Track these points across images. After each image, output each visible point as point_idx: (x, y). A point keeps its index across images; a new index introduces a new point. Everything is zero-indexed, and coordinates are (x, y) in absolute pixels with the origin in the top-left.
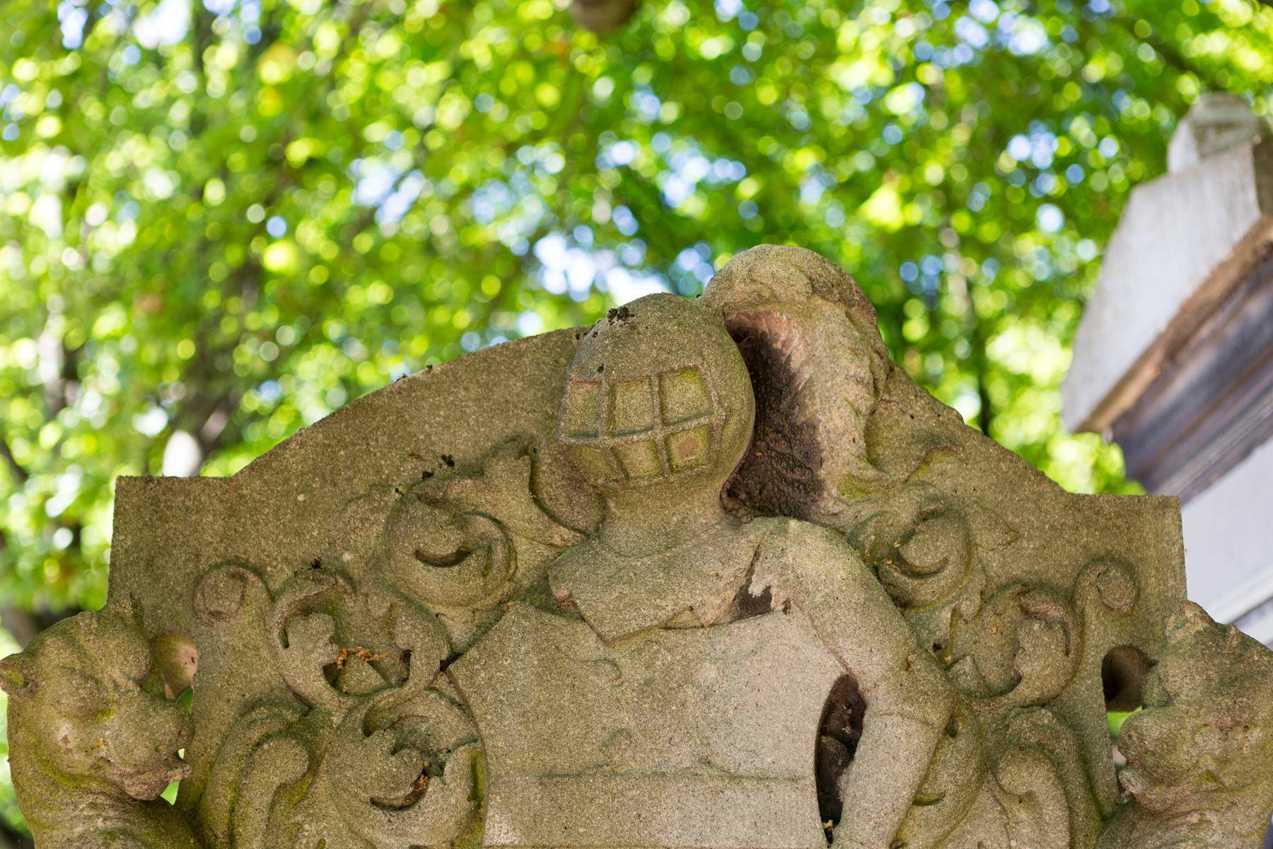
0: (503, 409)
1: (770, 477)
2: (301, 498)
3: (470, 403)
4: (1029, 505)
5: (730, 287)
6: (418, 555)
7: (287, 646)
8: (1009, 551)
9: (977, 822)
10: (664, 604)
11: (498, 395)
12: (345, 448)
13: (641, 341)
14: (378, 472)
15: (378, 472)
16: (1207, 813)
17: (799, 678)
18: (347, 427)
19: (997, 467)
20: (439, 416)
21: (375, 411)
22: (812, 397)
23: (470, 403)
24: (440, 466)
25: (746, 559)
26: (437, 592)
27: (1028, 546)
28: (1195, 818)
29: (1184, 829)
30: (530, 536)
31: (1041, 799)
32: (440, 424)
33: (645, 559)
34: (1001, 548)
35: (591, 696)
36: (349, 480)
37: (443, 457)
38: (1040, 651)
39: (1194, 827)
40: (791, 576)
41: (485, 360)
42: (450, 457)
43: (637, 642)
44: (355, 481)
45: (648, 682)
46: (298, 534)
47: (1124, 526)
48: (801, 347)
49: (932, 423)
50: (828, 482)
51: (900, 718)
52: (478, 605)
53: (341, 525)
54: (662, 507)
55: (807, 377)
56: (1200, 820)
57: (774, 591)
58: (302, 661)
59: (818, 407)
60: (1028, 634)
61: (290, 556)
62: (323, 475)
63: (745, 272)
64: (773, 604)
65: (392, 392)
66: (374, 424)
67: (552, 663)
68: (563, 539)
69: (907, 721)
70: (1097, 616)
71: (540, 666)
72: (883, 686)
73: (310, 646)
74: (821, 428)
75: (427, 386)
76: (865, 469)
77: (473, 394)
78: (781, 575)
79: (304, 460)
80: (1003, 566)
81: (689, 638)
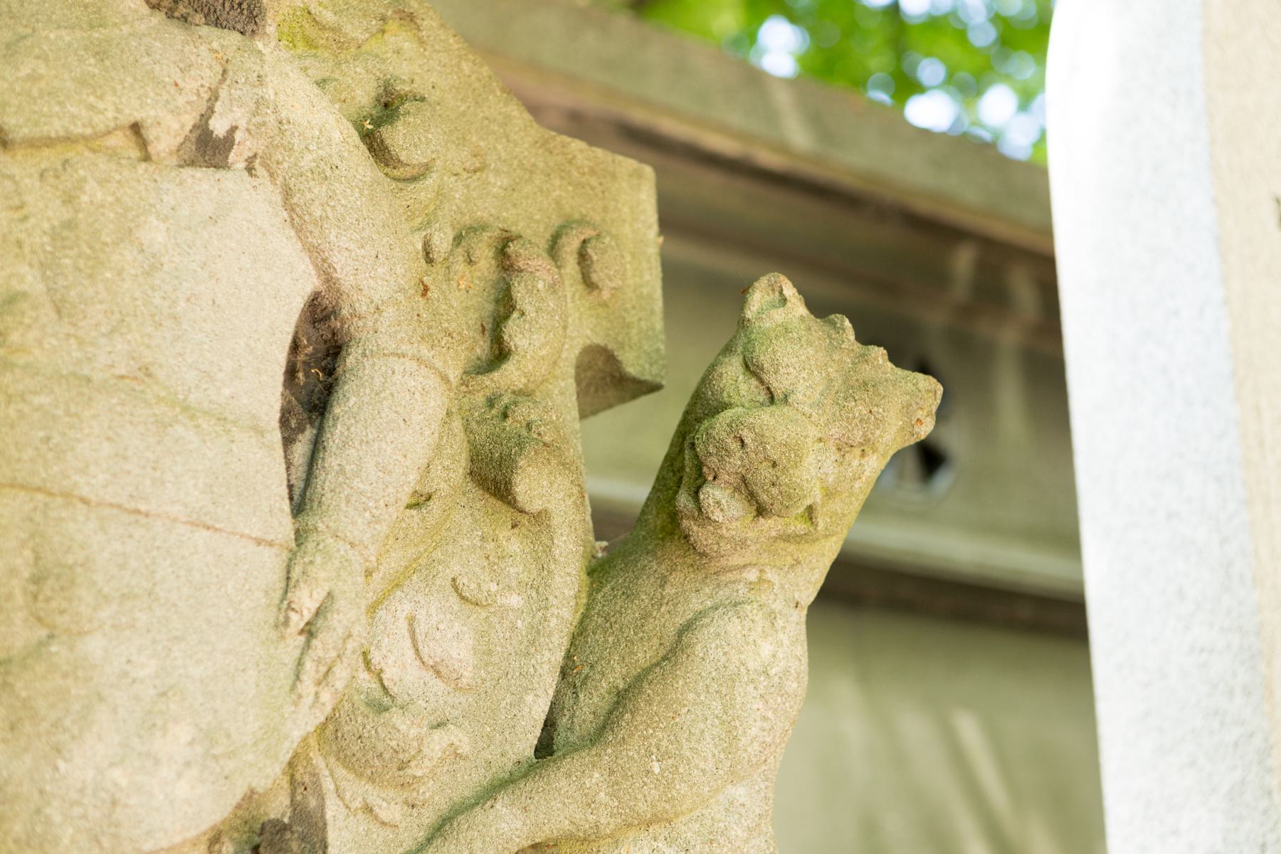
9: (450, 548)
10: (101, 105)
16: (767, 569)
19: (458, 66)
25: (210, 76)
27: (497, 183)
28: (752, 575)
29: (742, 590)
31: (556, 521)
33: (63, 32)
34: (465, 175)
39: (751, 586)
40: (271, 119)
43: (49, 158)
45: (69, 225)
47: (599, 189)
50: (270, 14)
51: (415, 364)
56: (760, 578)
57: (238, 136)
60: (530, 292)
64: (232, 156)
69: (424, 371)
72: (390, 312)
76: (326, 8)
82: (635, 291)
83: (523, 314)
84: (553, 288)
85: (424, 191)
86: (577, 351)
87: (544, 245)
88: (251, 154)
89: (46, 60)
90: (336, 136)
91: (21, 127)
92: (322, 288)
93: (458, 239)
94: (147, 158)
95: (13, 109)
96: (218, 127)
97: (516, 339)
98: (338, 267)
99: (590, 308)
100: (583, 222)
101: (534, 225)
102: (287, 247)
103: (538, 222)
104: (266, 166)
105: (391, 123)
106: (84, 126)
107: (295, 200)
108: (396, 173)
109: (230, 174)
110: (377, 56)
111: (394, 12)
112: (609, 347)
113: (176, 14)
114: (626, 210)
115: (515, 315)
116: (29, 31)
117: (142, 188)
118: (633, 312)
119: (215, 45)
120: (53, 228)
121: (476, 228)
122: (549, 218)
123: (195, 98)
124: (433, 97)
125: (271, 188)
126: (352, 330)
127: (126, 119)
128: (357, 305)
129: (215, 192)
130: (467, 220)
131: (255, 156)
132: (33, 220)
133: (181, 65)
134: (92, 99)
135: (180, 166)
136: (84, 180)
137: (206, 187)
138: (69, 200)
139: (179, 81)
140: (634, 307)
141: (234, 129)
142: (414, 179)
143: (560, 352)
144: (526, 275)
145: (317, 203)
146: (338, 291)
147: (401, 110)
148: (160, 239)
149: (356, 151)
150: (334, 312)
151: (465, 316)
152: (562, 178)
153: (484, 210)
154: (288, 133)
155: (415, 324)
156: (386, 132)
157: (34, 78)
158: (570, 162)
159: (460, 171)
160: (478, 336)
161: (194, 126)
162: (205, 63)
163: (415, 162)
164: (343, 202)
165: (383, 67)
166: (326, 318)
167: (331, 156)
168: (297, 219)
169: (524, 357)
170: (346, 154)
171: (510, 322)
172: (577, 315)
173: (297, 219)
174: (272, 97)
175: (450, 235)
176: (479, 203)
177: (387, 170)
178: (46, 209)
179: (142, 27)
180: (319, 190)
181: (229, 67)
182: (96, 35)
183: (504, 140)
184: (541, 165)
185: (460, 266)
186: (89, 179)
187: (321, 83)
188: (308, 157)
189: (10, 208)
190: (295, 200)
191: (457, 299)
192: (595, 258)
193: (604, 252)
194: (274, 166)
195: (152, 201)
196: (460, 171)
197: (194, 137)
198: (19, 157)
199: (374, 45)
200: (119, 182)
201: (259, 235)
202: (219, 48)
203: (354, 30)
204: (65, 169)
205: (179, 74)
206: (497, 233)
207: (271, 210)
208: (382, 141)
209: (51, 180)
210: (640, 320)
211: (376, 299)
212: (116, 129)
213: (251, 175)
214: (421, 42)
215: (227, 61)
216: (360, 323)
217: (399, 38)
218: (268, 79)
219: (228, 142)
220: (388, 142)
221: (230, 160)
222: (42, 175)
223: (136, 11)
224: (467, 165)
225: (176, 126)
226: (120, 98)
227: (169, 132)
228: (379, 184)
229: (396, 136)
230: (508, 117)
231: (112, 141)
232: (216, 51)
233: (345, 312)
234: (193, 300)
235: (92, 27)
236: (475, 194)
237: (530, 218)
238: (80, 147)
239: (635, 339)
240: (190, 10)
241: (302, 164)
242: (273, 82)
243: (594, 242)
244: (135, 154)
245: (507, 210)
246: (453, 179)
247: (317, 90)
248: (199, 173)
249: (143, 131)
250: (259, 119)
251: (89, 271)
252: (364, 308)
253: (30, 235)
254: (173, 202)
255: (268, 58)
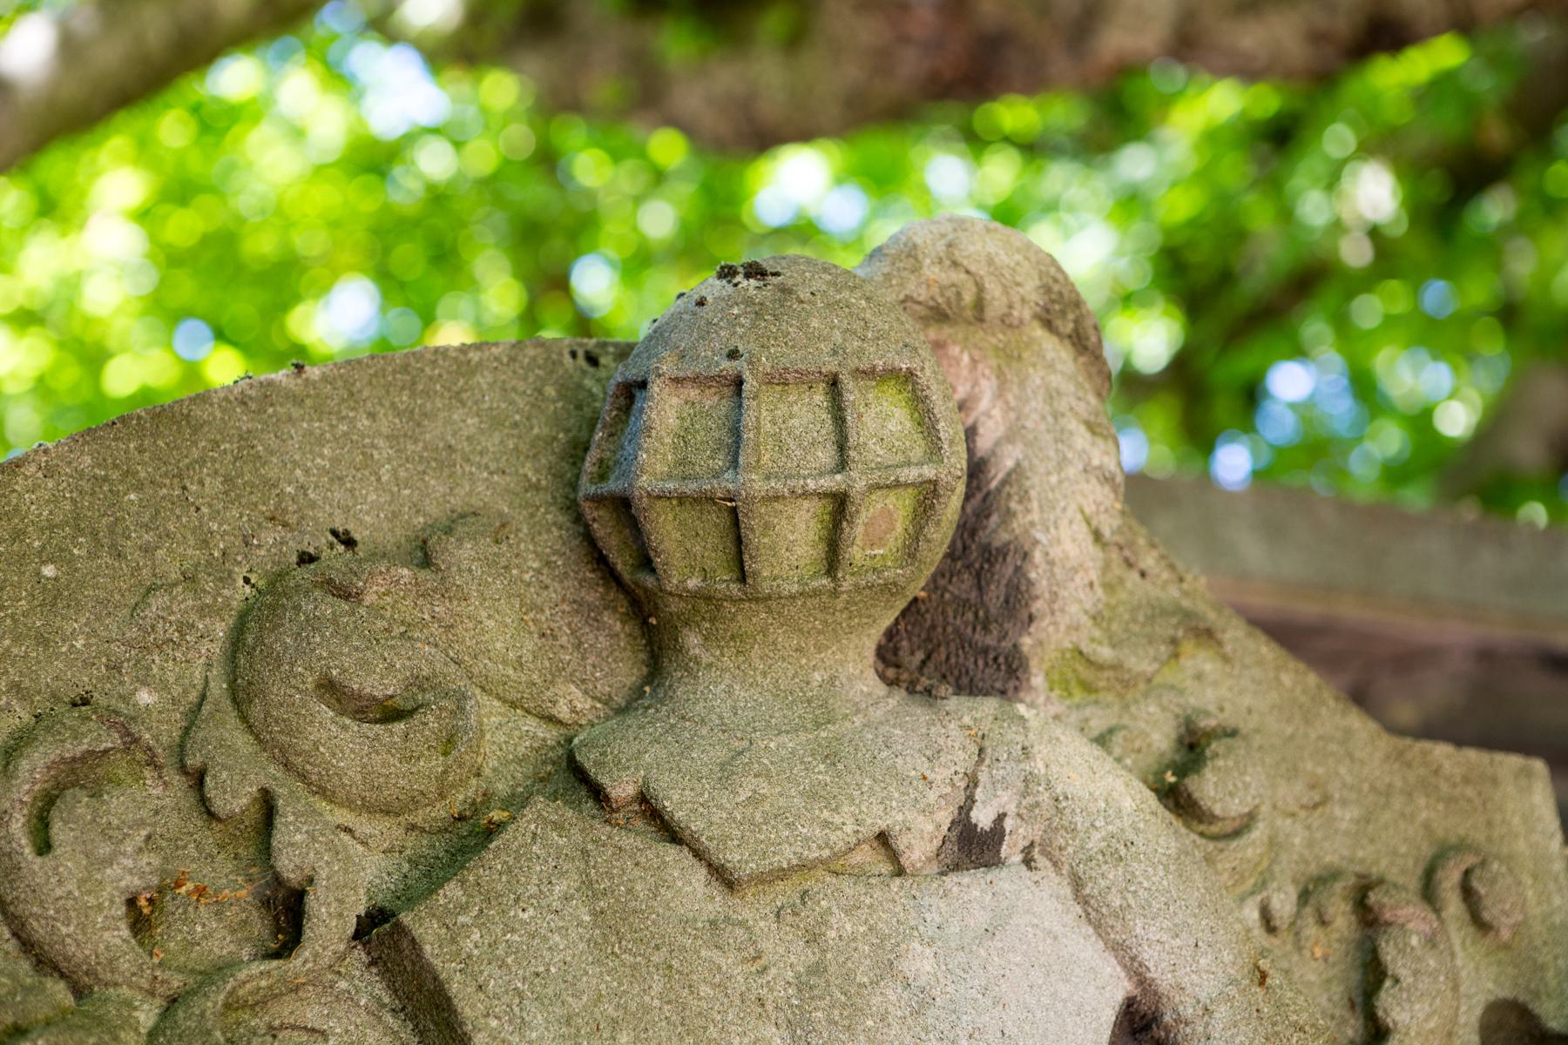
0: (444, 459)
1: (576, 779)
2: (49, 571)
3: (381, 442)
4: (1333, 747)
5: (915, 270)
6: (330, 689)
7: (44, 846)
8: (1316, 819)
10: (837, 820)
11: (433, 432)
12: (139, 487)
13: (809, 314)
14: (205, 543)
15: (205, 543)
17: (1064, 990)
18: (141, 451)
19: (1277, 678)
20: (322, 456)
21: (196, 430)
22: (1024, 498)
23: (381, 442)
24: (332, 547)
25: (962, 759)
26: (354, 775)
27: (1346, 816)
30: (514, 695)
32: (323, 471)
33: (784, 738)
34: (1303, 814)
35: (705, 990)
36: (147, 550)
37: (334, 533)
38: (1424, 984)
40: (1045, 798)
41: (405, 368)
42: (347, 532)
43: (785, 893)
44: (160, 553)
45: (817, 969)
46: (43, 641)
47: (1477, 801)
48: (996, 413)
49: (1174, 591)
50: (1034, 664)
52: (418, 818)
53: (132, 633)
54: (799, 650)
55: (1009, 463)
57: (1008, 824)
58: (82, 882)
59: (1035, 516)
60: (1402, 951)
61: (27, 683)
62: (94, 534)
63: (941, 246)
65: (226, 399)
66: (195, 454)
67: (615, 925)
68: (573, 710)
70: (1463, 943)
71: (595, 925)
72: (1222, 1013)
73: (104, 850)
74: (1038, 556)
75: (298, 401)
76: (1100, 643)
77: (384, 426)
78: (1025, 794)
79: (54, 500)
80: (1310, 844)
81: (877, 894)
82: (1543, 921)
83: (1397, 981)
84: (1431, 942)
85: (1252, 846)
86: (1478, 1011)
87: (1414, 884)
88: (1026, 843)
89: (768, 777)
90: (1128, 804)
91: (747, 862)
92: (1136, 992)
93: (1304, 897)
94: (900, 872)
95: (736, 842)
96: (983, 817)
97: (1394, 1014)
98: (1151, 965)
99: (1487, 955)
100: (1461, 847)
101: (1400, 861)
102: (1086, 949)
103: (1404, 856)
104: (1046, 854)
105: (1198, 772)
106: (820, 847)
107: (1087, 891)
108: (1214, 829)
109: (1004, 873)
110: (1172, 687)
111: (1186, 632)
112: (1521, 999)
113: (919, 688)
114: (1516, 820)
115: (1388, 983)
116: (746, 743)
117: (899, 909)
118: (1545, 950)
119: (967, 720)
120: (798, 976)
121: (1326, 878)
122: (1419, 848)
123: (949, 789)
124: (1246, 726)
125: (1057, 879)
126: (1179, 1038)
127: (868, 831)
128: (1181, 1008)
129: (988, 898)
130: (1313, 869)
131: (1032, 844)
132: (773, 971)
133: (928, 753)
134: (826, 814)
135: (943, 874)
136: (829, 911)
137: (977, 893)
138: (813, 938)
139: (927, 773)
140: (1545, 943)
141: (1001, 818)
142: (1236, 833)
143: (1454, 1020)
144: (1394, 931)
145: (1114, 890)
146: (1156, 993)
147: (1208, 753)
148: (928, 968)
149: (1153, 820)
150: (1155, 1019)
151: (1328, 990)
152: (1427, 796)
153: (1333, 853)
154: (1067, 811)
155: (1254, 1023)
156: (1192, 784)
157: (755, 800)
158: (1436, 772)
159: (1296, 809)
160: (1347, 1014)
161: (953, 823)
162: (957, 745)
163: (1233, 814)
164: (1146, 884)
165: (1182, 701)
166: (1146, 1028)
167: (1122, 830)
168: (1093, 914)
169: (1407, 1034)
170: (1141, 825)
171: (1383, 994)
172: (1472, 965)
173: (1093, 914)
174: (1043, 771)
175: (1292, 893)
176: (1327, 844)
177: (1202, 828)
178: (787, 955)
179: (877, 714)
180: (1114, 874)
181: (987, 743)
182: (824, 734)
183: (1347, 761)
184: (1399, 783)
185: (1311, 930)
186: (834, 909)
187: (1102, 740)
188: (1096, 836)
189: (745, 960)
190: (1087, 891)
191: (1311, 972)
192: (1483, 891)
193: (1493, 881)
194: (1057, 853)
195: (913, 923)
196: (1296, 809)
197: (954, 835)
198: (749, 898)
199: (1168, 675)
200: (871, 906)
201: (1049, 941)
202: (971, 723)
203: (1140, 663)
204: (804, 904)
205: (926, 765)
206: (1352, 880)
207: (1060, 907)
208: (1189, 796)
209: (789, 919)
210: (1556, 958)
211: (1203, 997)
212: (859, 843)
213: (1030, 868)
214: (1226, 659)
215: (983, 737)
216: (1188, 1030)
217: (1199, 660)
218: (1035, 750)
219: (997, 833)
220: (1196, 795)
221: (1003, 855)
222: (778, 915)
223: (870, 694)
224: (1305, 800)
225: (930, 827)
226: (858, 806)
227: (922, 836)
228: (1187, 854)
229: (1207, 787)
230: (1348, 732)
231: (856, 858)
232: (969, 728)
233: (1168, 1018)
234: (976, 1035)
235: (818, 725)
236: (1319, 835)
237: (1392, 854)
238: (820, 873)
239: (1553, 983)
240: (934, 681)
241: (1090, 845)
242: (1041, 751)
243: (1478, 872)
244: (886, 868)
245: (1363, 848)
246: (1289, 821)
247: (1097, 751)
248: (966, 878)
249: (891, 841)
250: (1030, 800)
251: (846, 1023)
252: (1190, 1011)
253: (771, 990)
254: (938, 920)
255: (1034, 723)
